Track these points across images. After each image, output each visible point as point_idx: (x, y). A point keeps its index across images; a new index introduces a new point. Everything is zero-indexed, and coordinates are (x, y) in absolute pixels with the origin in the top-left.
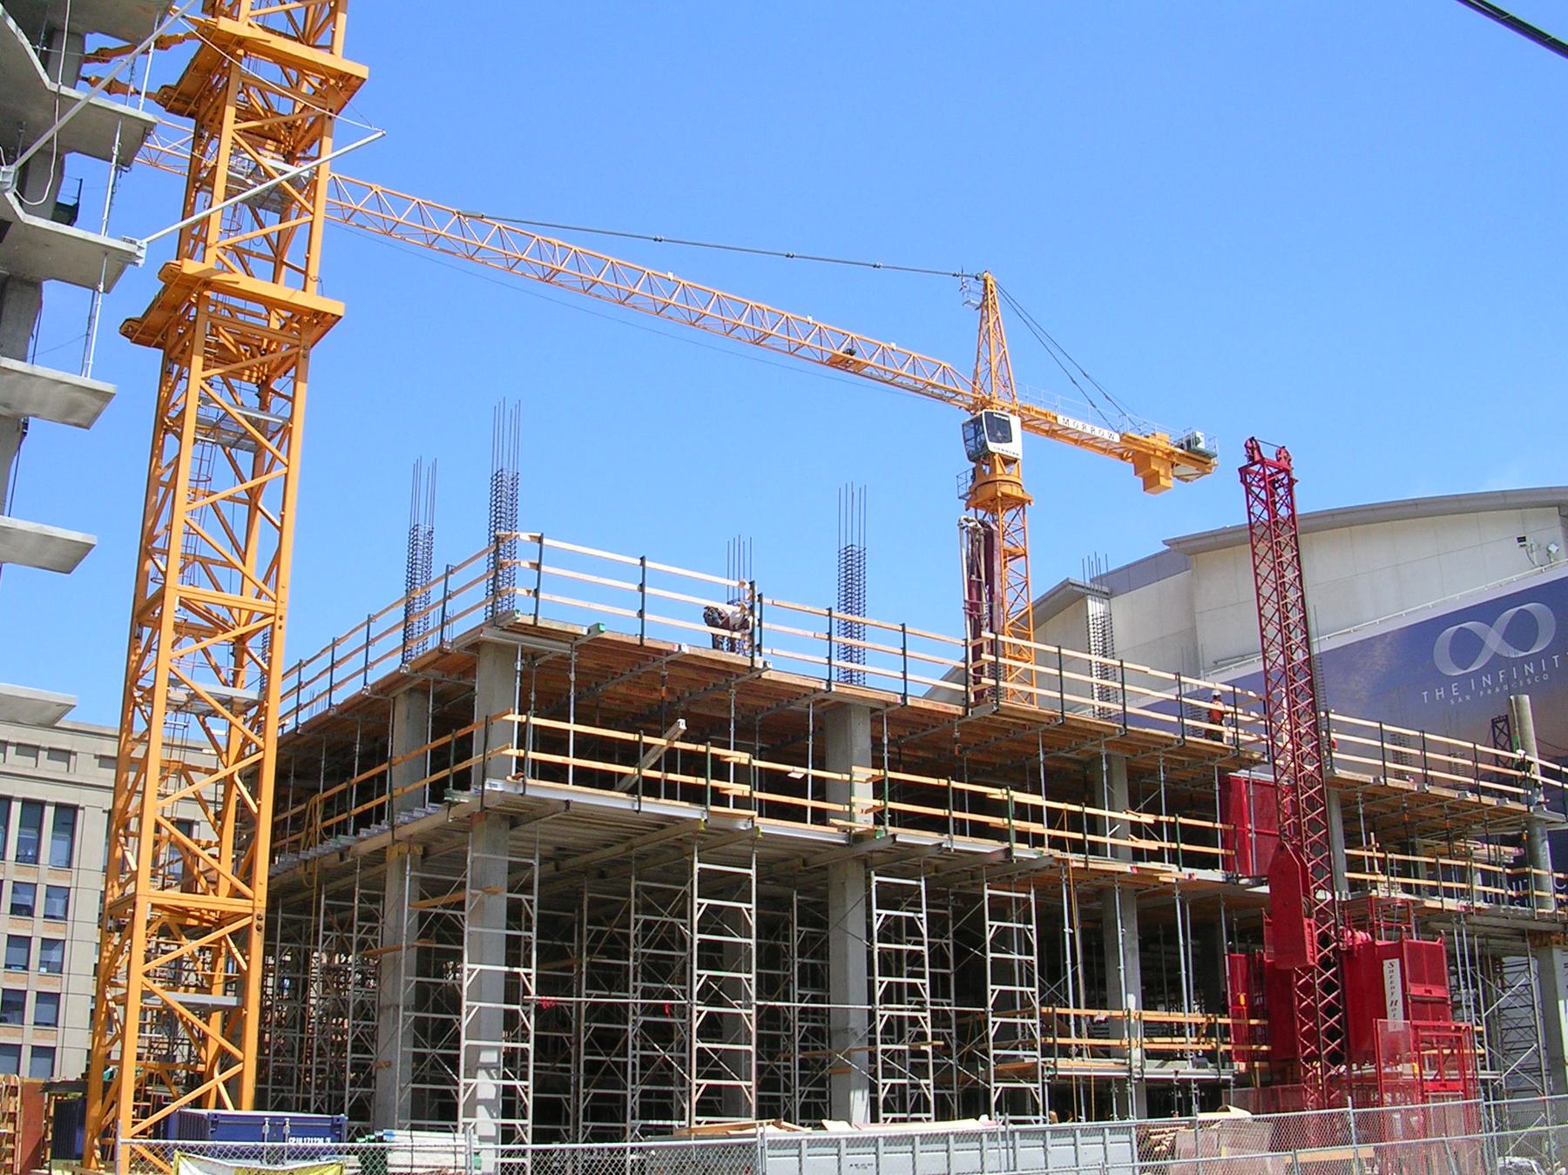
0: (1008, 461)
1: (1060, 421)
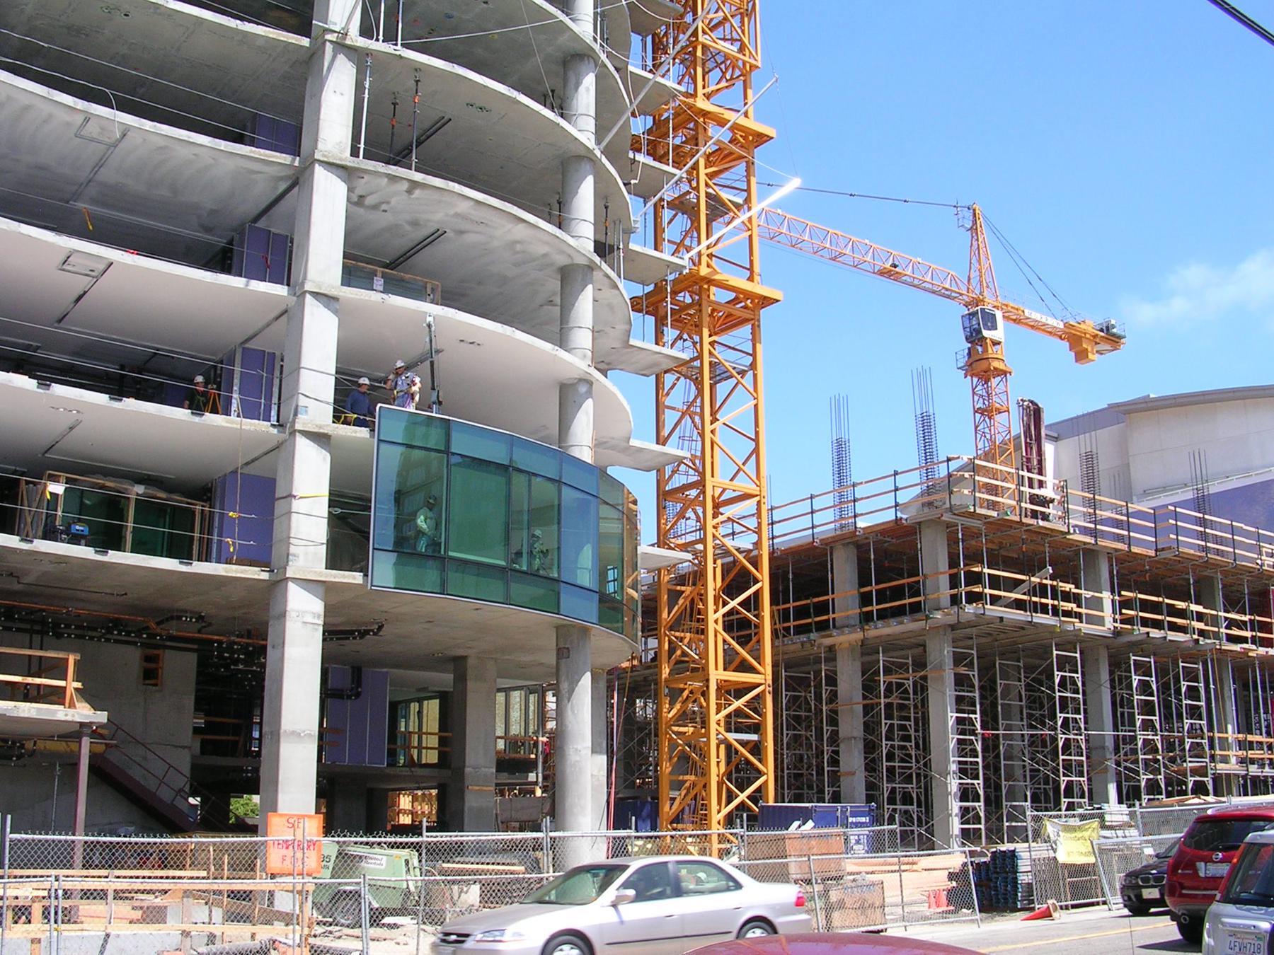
0: (996, 343)
1: (1027, 314)
